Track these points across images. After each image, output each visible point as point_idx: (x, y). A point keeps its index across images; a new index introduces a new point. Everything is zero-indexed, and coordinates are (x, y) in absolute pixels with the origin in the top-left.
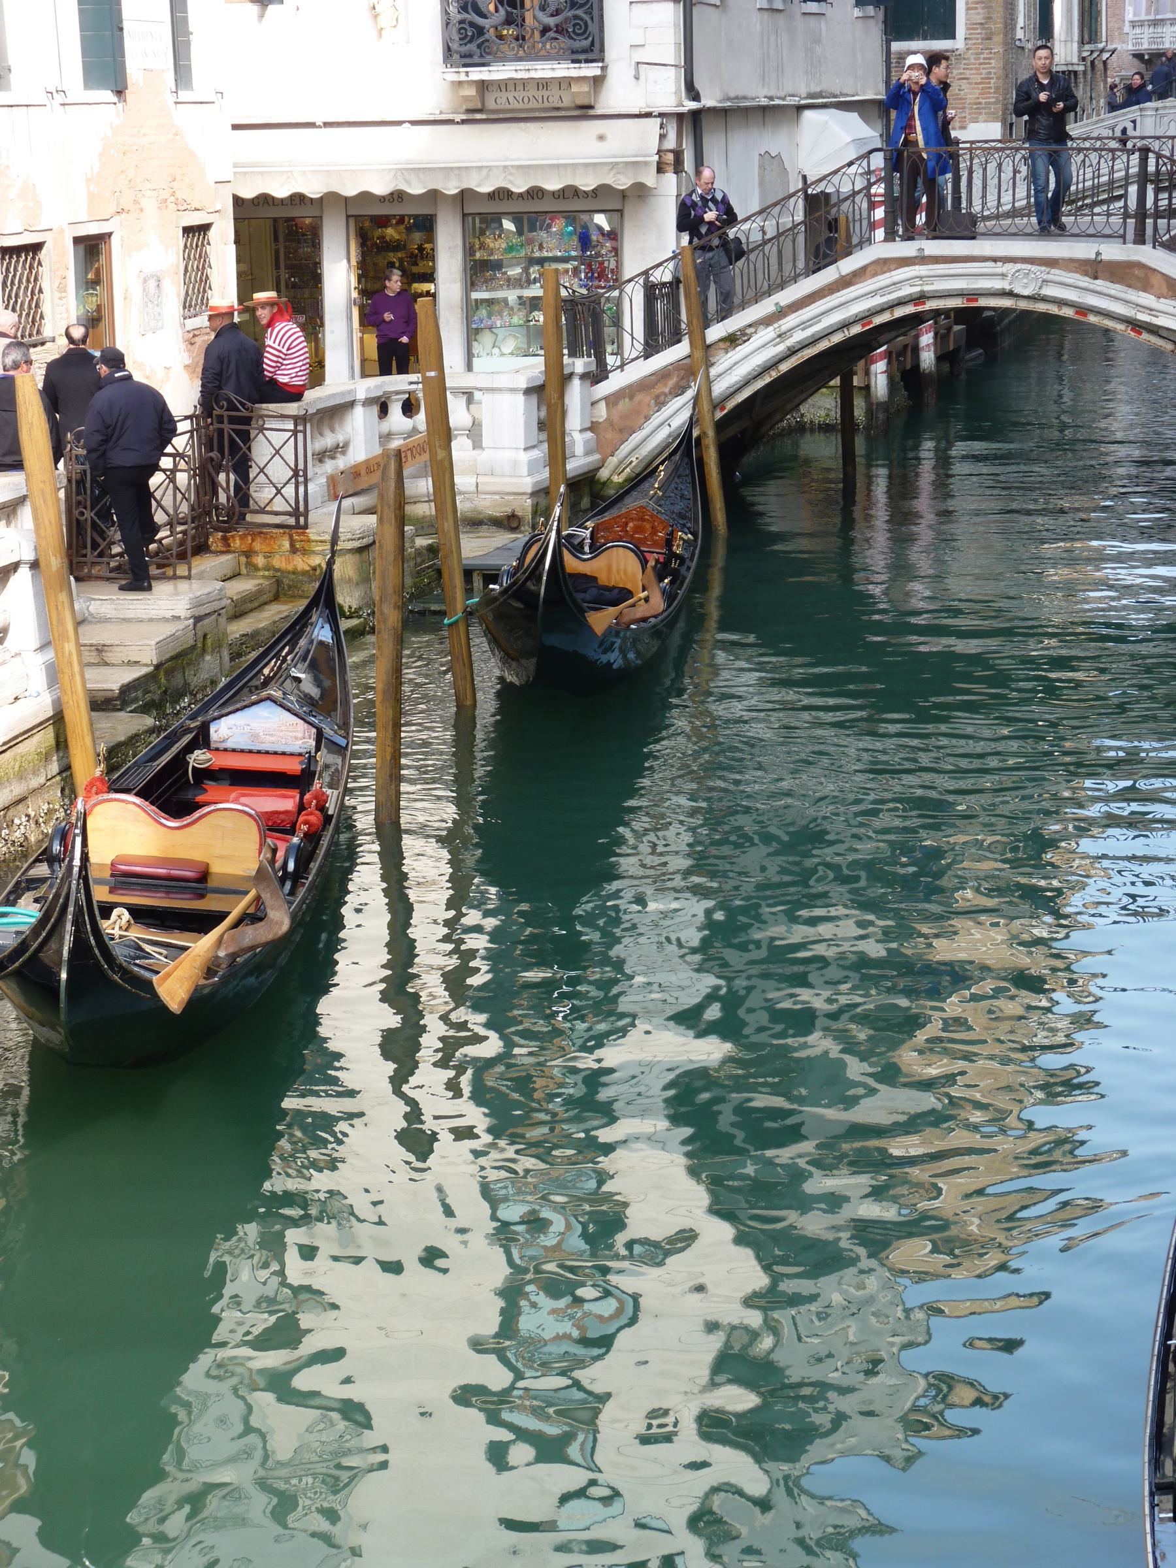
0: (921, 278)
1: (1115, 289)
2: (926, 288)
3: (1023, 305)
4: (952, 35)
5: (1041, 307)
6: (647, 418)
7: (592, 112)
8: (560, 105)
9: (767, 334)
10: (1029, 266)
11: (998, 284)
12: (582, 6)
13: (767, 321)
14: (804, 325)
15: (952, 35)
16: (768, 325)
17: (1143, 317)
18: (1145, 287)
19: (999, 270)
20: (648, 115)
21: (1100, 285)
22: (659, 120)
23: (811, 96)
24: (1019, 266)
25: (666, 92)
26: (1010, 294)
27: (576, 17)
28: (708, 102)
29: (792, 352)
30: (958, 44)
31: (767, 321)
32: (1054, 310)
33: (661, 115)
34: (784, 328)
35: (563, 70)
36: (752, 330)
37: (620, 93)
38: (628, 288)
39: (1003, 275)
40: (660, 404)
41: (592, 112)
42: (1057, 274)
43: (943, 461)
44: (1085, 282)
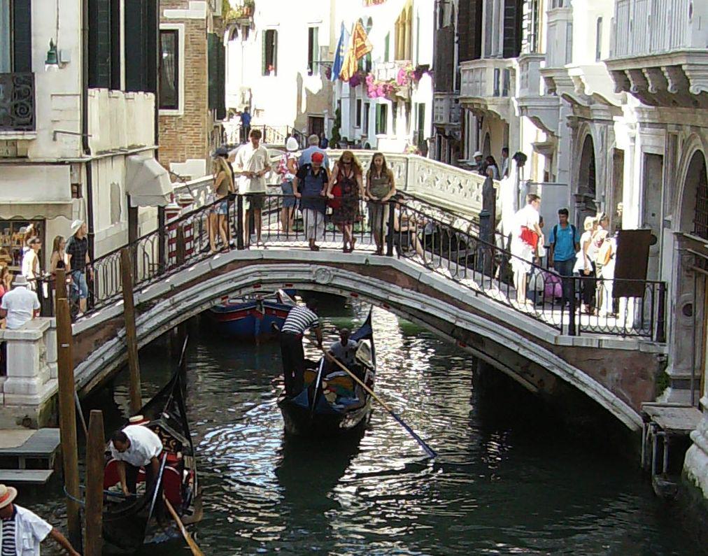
0: (260, 272)
1: (376, 281)
2: (263, 278)
3: (320, 289)
4: (176, 107)
5: (330, 290)
6: (90, 354)
7: (27, 160)
8: (7, 155)
9: (167, 303)
10: (325, 267)
11: (306, 277)
12: (25, 97)
13: (165, 296)
14: (188, 299)
15: (176, 107)
16: (165, 298)
17: (392, 298)
18: (393, 281)
19: (308, 269)
20: (63, 163)
21: (366, 279)
22: (69, 167)
23: (130, 148)
24: (320, 267)
25: (71, 147)
26: (314, 283)
27: (22, 104)
28: (93, 156)
29: (179, 314)
30: (180, 112)
31: (165, 296)
32: (338, 292)
33: (70, 163)
34: (176, 300)
35: (12, 135)
36: (155, 301)
37: (42, 145)
38: (99, 267)
39: (310, 272)
40: (98, 344)
41: (27, 160)
42: (342, 272)
43: (503, 246)
44: (359, 277)
